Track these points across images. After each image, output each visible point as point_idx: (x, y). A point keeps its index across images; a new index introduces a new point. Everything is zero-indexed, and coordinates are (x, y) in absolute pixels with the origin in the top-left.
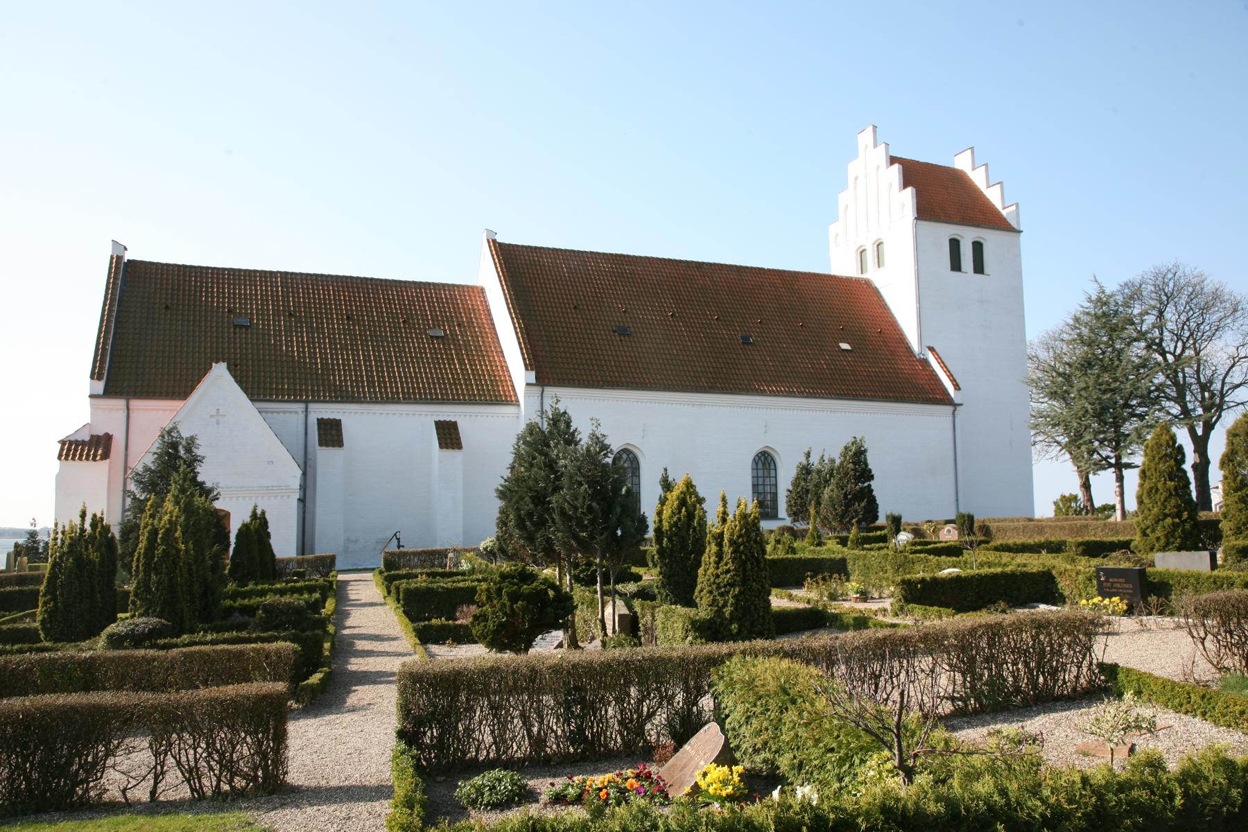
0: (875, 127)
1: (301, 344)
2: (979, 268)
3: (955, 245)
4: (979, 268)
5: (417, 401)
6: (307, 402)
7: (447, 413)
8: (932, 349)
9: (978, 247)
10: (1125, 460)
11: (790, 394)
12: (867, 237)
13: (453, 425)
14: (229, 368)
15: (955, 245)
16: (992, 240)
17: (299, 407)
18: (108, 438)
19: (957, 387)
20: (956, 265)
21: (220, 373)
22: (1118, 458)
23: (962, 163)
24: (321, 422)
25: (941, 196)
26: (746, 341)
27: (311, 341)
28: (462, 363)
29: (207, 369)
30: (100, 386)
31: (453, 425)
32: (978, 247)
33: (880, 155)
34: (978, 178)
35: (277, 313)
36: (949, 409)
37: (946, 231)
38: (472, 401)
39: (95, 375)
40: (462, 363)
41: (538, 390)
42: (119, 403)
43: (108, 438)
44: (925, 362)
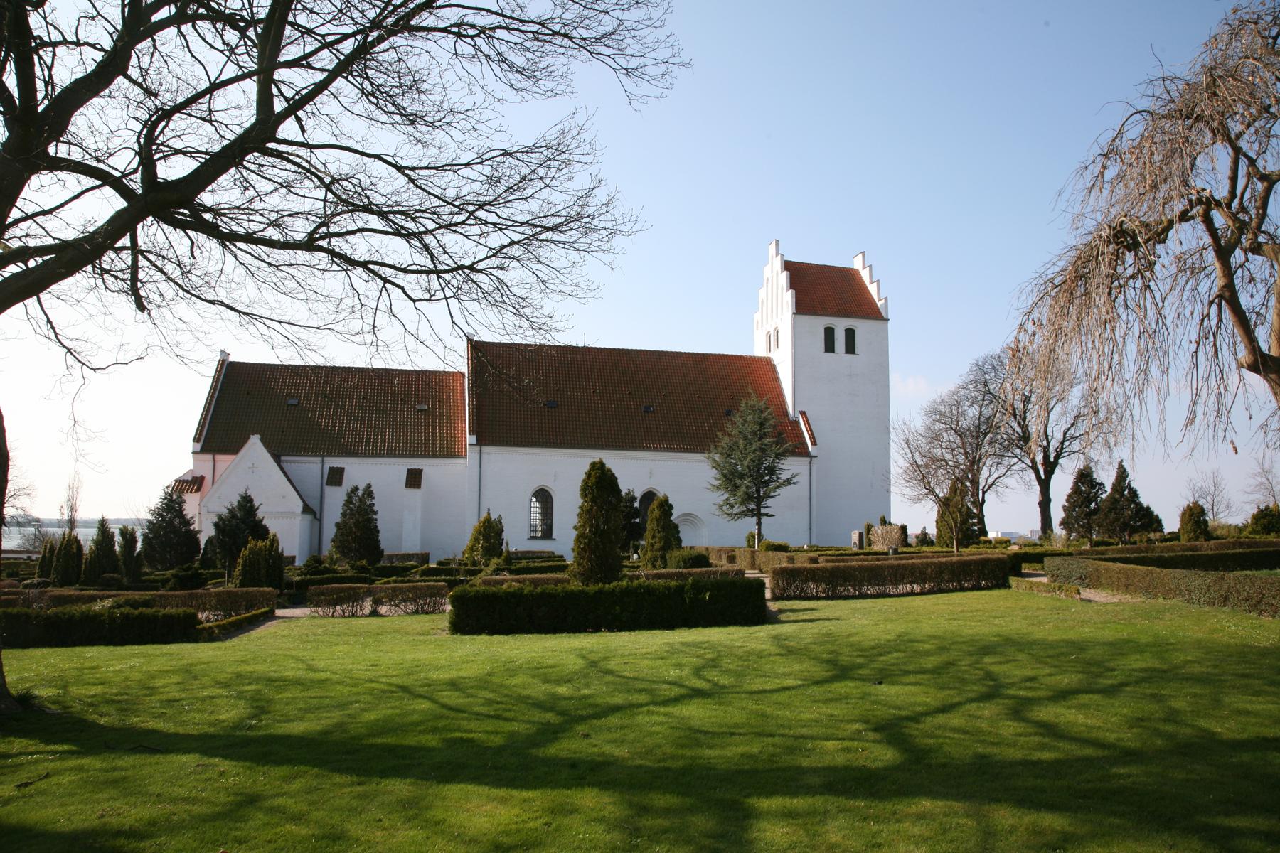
0: (777, 242)
1: (328, 417)
2: (850, 348)
3: (829, 333)
4: (850, 348)
5: (395, 456)
6: (323, 456)
7: (415, 463)
8: (803, 413)
9: (850, 334)
10: (763, 511)
11: (671, 450)
12: (764, 327)
13: (419, 472)
14: (262, 440)
15: (829, 333)
16: (863, 328)
17: (318, 460)
18: (202, 478)
19: (814, 443)
20: (830, 347)
21: (255, 440)
22: (759, 509)
23: (857, 264)
24: (331, 469)
25: (827, 295)
26: (647, 410)
27: (335, 414)
28: (434, 428)
29: (246, 440)
30: (199, 446)
31: (419, 472)
32: (850, 334)
33: (777, 264)
34: (865, 275)
35: (317, 396)
36: (807, 460)
37: (818, 324)
38: (434, 455)
39: (196, 439)
40: (434, 428)
41: (477, 448)
42: (210, 457)
43: (202, 478)
44: (797, 423)
